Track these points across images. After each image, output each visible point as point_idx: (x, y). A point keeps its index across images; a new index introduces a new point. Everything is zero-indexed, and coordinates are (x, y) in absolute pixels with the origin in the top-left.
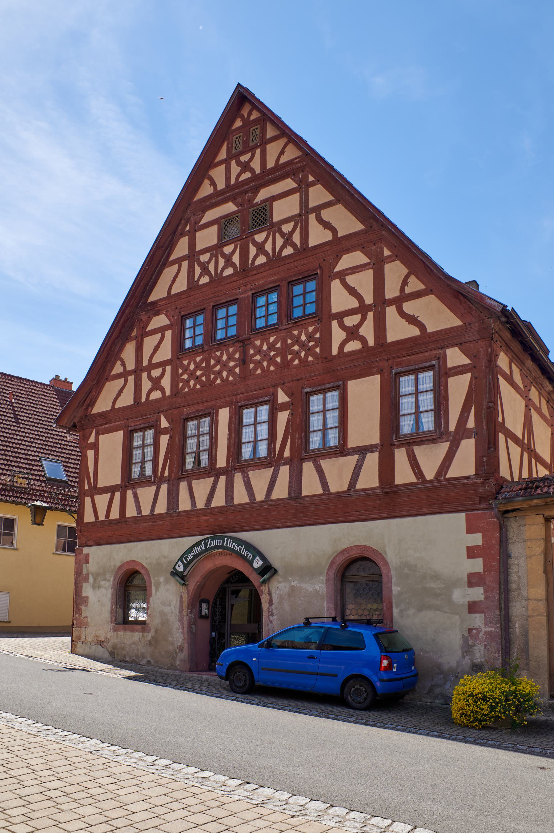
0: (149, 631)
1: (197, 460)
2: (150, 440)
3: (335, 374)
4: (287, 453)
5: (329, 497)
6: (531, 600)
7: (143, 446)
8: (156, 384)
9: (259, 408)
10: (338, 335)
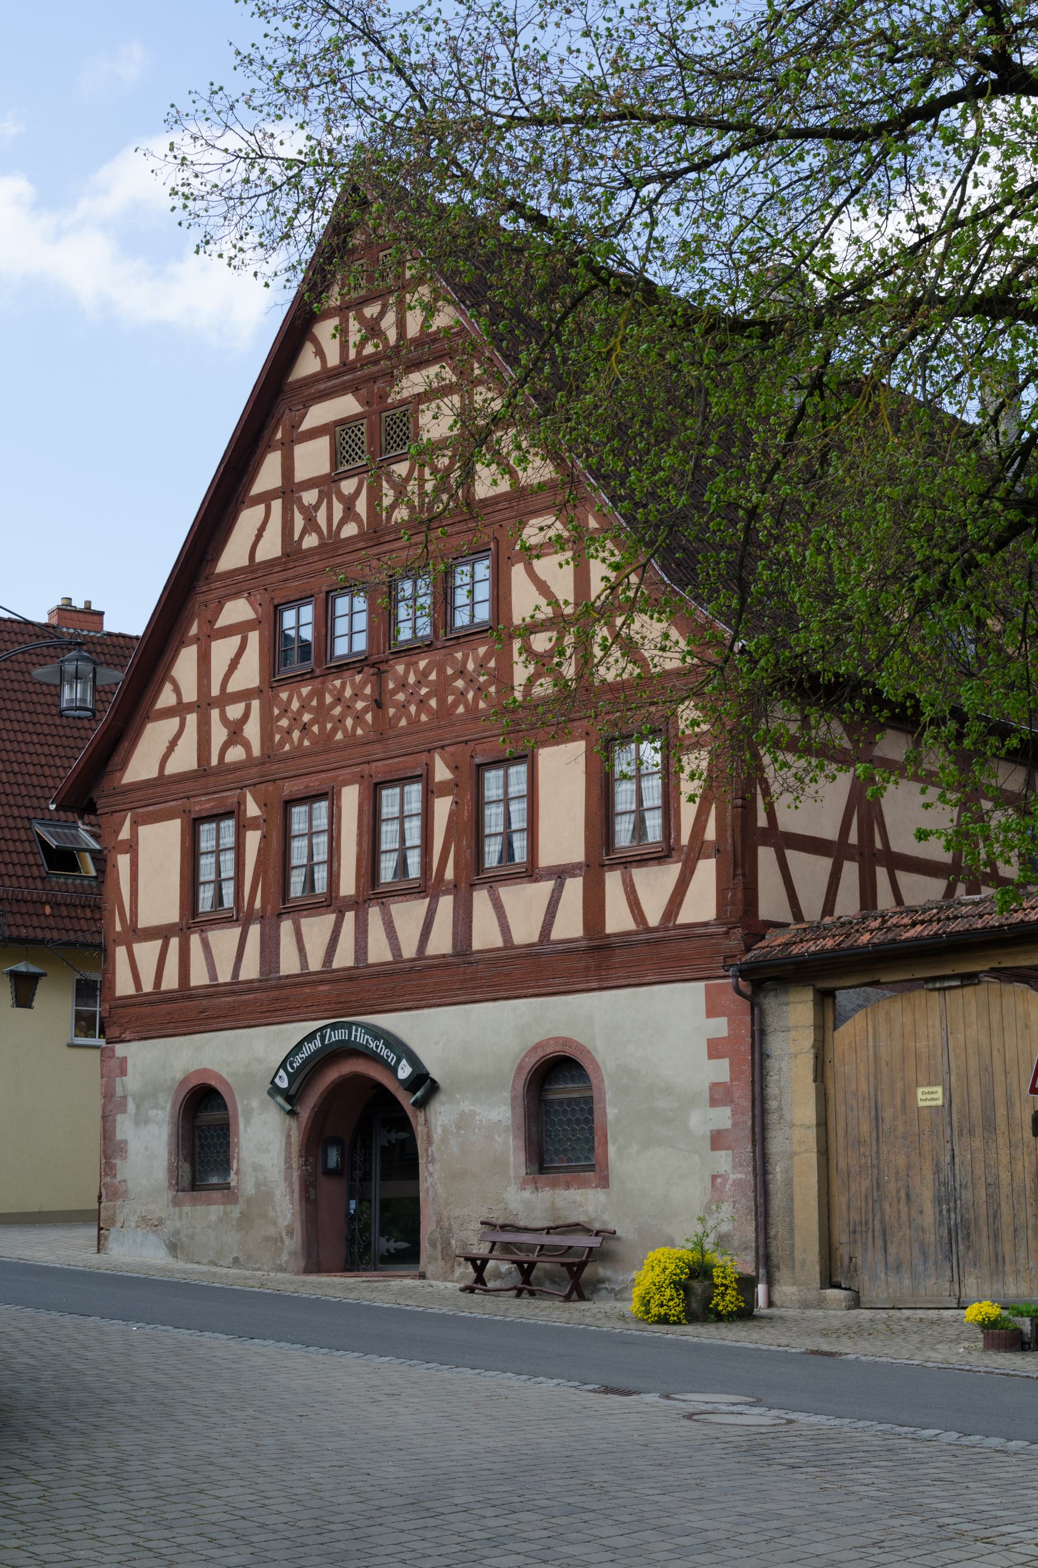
0: (235, 1202)
1: (310, 882)
3: (519, 733)
4: (449, 874)
5: (512, 952)
7: (218, 852)
8: (235, 732)
9: (407, 788)
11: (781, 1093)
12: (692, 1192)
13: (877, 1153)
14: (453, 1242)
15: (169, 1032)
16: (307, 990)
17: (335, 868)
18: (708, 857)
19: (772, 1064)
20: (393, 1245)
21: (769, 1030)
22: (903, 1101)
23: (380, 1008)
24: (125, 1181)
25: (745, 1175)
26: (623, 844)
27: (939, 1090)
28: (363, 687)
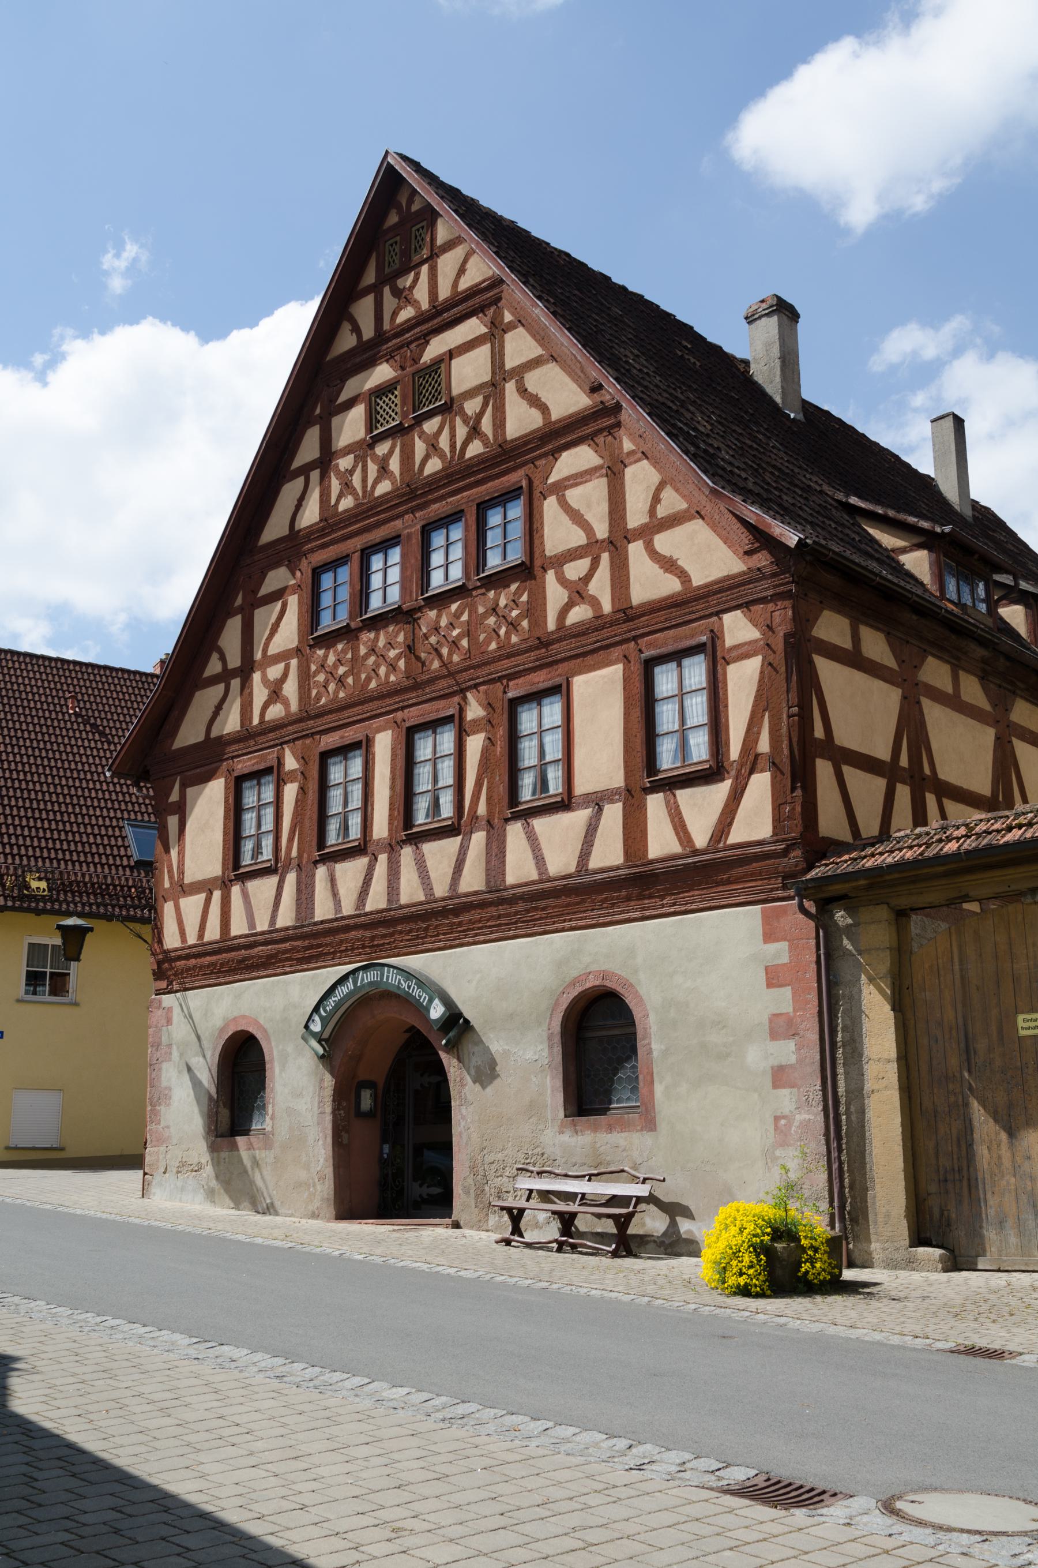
2: (268, 794)
10: (555, 595)
18: (762, 771)
20: (425, 1191)
22: (1000, 1031)
24: (168, 1127)
25: (813, 1116)
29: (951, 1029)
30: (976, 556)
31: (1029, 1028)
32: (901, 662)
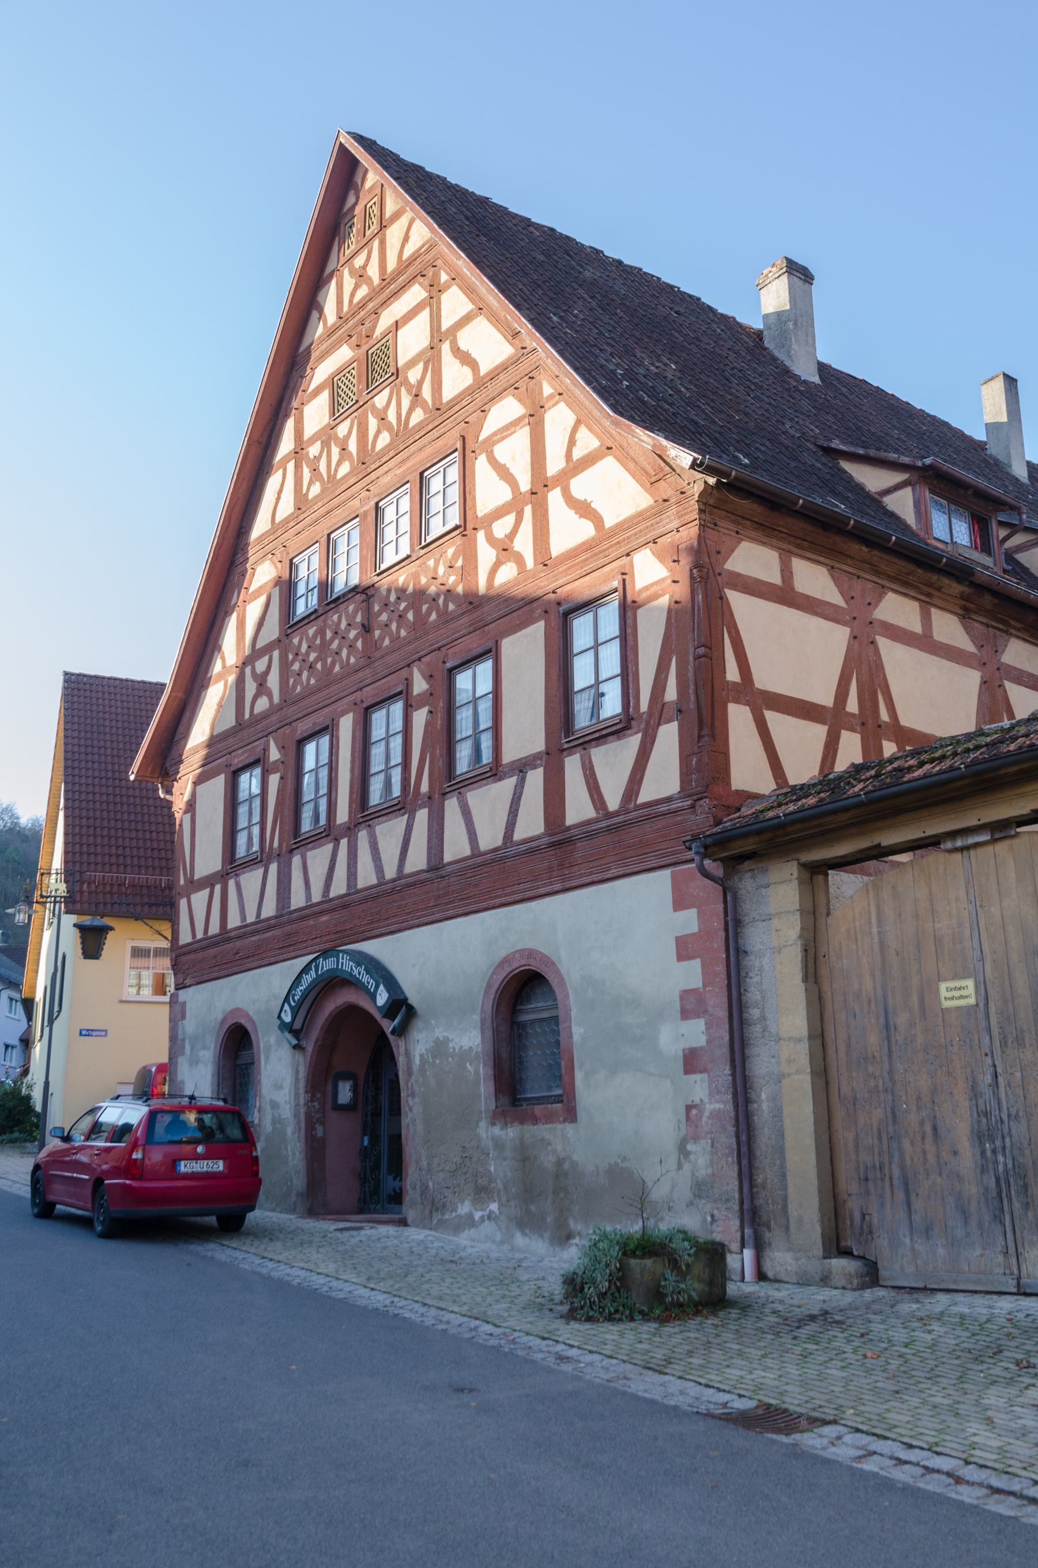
4: (425, 787)
5: (479, 860)
6: (785, 1040)
10: (486, 555)
11: (763, 997)
12: (663, 1126)
13: (891, 1072)
14: (431, 1184)
15: (215, 975)
16: (311, 922)
17: (333, 797)
18: (669, 721)
19: (752, 962)
21: (747, 920)
23: (369, 934)
25: (721, 1105)
26: (583, 725)
27: (970, 983)
28: (355, 617)
29: (870, 1001)
30: (970, 492)
31: (952, 998)
32: (850, 599)
